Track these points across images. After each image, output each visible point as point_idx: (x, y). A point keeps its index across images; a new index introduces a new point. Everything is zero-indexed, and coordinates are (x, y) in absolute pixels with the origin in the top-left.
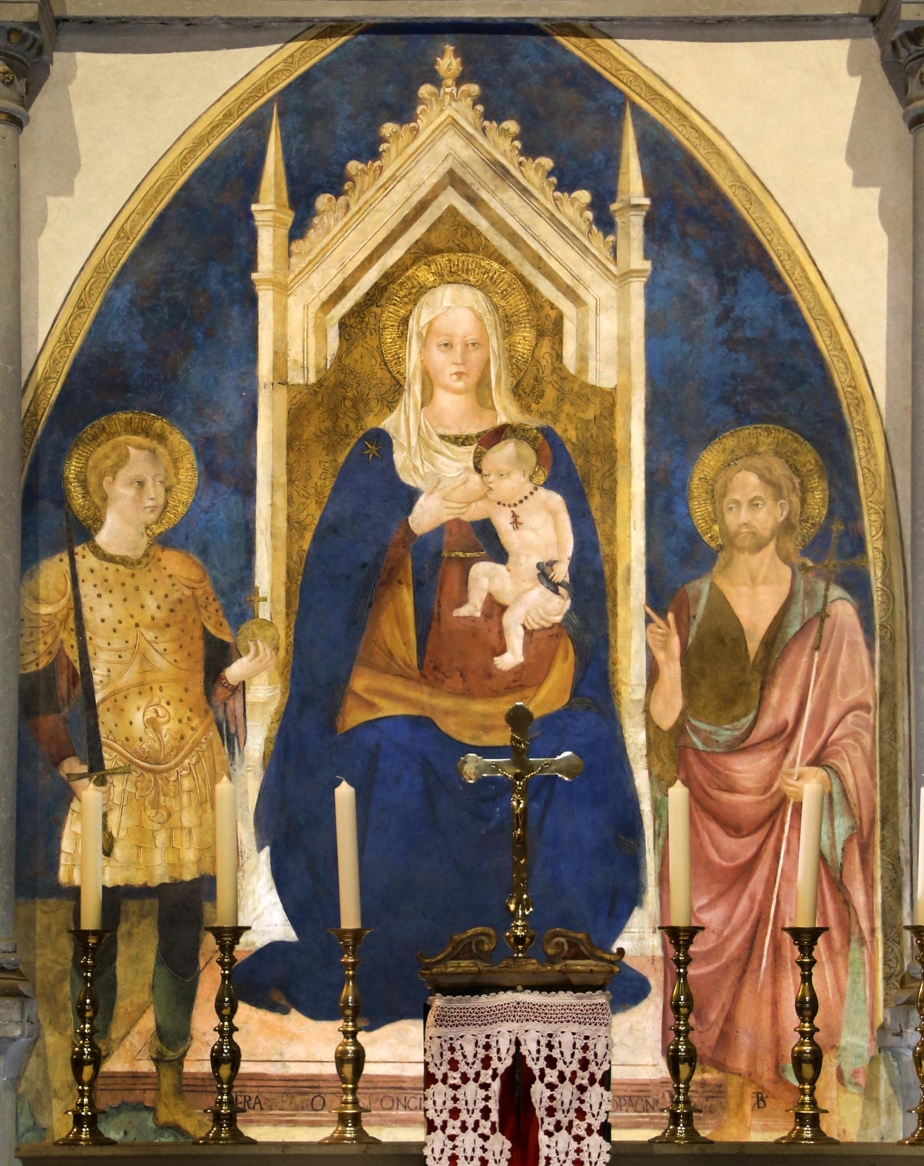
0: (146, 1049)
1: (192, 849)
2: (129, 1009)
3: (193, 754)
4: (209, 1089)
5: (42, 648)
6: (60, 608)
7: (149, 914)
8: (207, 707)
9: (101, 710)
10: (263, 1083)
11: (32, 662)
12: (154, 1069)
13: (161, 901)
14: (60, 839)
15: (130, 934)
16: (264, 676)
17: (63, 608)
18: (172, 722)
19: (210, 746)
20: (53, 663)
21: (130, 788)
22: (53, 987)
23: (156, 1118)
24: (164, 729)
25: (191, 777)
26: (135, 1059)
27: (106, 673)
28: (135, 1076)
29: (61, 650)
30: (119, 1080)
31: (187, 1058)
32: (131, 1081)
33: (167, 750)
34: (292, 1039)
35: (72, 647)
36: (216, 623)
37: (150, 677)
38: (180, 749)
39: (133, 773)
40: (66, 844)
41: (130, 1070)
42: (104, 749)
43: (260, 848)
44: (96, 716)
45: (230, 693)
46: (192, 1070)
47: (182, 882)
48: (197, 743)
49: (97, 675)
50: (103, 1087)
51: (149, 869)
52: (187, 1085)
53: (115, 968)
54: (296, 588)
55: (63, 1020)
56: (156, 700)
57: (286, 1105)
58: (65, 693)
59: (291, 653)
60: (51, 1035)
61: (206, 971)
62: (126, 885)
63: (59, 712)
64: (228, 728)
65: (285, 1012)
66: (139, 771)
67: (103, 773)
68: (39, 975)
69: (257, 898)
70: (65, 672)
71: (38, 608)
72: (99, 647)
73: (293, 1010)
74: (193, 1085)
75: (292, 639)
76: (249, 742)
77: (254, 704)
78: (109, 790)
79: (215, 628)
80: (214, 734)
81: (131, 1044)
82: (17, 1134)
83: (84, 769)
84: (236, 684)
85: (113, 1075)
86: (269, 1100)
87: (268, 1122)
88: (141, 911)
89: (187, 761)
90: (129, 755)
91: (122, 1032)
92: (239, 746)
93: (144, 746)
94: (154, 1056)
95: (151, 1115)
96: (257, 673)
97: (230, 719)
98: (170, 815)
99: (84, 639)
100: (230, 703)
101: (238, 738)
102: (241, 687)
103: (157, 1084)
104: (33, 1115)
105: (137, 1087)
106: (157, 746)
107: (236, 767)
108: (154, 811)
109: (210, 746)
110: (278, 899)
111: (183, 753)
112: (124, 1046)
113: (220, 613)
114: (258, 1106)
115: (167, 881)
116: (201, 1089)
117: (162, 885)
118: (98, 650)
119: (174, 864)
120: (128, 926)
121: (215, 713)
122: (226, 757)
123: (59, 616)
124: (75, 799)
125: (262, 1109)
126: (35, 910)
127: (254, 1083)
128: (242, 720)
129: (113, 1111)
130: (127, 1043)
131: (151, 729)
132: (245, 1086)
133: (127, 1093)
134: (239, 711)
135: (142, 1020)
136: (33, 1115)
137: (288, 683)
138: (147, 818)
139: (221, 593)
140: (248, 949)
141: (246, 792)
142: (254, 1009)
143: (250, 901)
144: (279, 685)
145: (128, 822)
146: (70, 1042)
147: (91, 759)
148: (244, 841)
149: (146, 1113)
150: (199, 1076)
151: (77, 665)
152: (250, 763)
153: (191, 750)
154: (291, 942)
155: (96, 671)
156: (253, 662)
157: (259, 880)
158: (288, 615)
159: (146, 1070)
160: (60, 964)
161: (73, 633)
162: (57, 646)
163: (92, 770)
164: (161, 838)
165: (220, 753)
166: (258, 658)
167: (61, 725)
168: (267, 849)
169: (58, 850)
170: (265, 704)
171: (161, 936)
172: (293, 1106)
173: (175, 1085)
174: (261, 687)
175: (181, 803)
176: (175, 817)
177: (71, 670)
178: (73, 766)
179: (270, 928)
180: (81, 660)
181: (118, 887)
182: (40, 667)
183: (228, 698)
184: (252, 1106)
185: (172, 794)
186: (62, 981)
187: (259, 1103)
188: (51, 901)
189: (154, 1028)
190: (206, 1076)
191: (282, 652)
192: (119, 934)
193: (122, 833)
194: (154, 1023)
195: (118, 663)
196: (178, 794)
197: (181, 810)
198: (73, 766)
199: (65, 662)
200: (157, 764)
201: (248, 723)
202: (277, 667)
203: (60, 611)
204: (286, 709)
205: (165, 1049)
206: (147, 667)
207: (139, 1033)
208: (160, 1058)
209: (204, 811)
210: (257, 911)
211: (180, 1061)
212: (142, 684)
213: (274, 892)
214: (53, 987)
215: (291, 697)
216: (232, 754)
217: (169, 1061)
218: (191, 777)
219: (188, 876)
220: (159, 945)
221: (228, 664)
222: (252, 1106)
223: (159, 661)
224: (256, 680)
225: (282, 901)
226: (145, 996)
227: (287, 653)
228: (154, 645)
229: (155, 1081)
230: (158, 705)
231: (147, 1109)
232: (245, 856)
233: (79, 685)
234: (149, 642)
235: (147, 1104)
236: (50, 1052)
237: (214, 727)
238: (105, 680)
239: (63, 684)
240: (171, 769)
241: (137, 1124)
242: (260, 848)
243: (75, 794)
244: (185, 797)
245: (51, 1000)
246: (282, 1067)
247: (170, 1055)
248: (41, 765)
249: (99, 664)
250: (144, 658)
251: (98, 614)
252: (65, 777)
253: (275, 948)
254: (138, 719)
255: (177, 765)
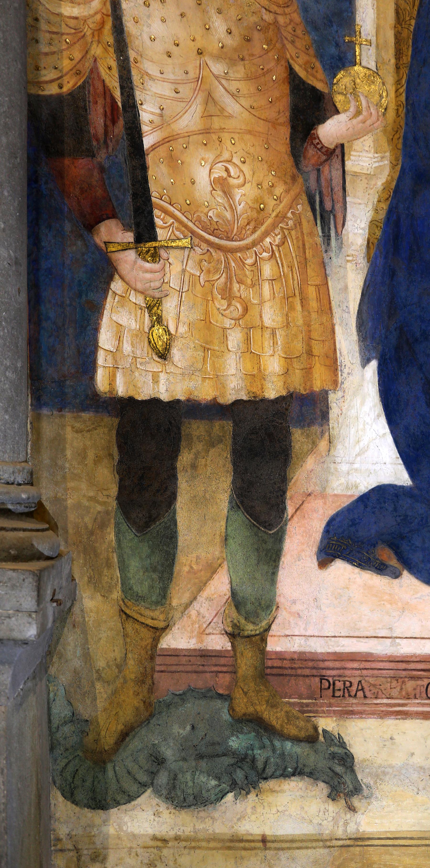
0: (218, 620)
1: (276, 357)
2: (195, 567)
3: (277, 231)
4: (299, 672)
5: (66, 64)
6: (92, 12)
7: (220, 441)
8: (295, 171)
9: (150, 160)
10: (368, 665)
11: (52, 81)
12: (228, 646)
13: (236, 424)
14: (96, 330)
15: (194, 466)
16: (367, 142)
17: (96, 13)
18: (247, 185)
19: (298, 223)
20: (82, 87)
21: (192, 269)
22: (92, 533)
23: (231, 709)
24: (238, 194)
25: (273, 261)
26: (202, 633)
27: (158, 111)
28: (204, 654)
29: (94, 70)
30: (184, 660)
31: (271, 633)
32: (200, 661)
33: (242, 222)
34: (403, 609)
35: (110, 68)
36: (306, 63)
37: (217, 123)
38: (259, 223)
39: (197, 248)
40: (105, 339)
41: (198, 646)
42: (156, 212)
43: (365, 362)
44: (144, 168)
45: (324, 157)
46: (278, 649)
47: (264, 400)
48: (282, 217)
49: (145, 111)
50: (162, 668)
51: (219, 379)
52: (272, 667)
53: (175, 513)
54: (407, 34)
55: (106, 579)
56: (226, 155)
57: (395, 693)
58: (101, 131)
59: (403, 115)
60: (92, 598)
61: (295, 518)
62: (188, 400)
63: (93, 156)
64: (321, 202)
65: (396, 575)
66: (204, 246)
67: (154, 244)
68: (72, 517)
69: (361, 426)
70: (101, 101)
71: (60, 6)
72: (148, 74)
73: (405, 574)
74: (280, 668)
75: (403, 98)
76: (349, 223)
77: (356, 175)
78: (163, 268)
79: (306, 70)
80: (302, 207)
81: (199, 613)
82: (50, 728)
83: (129, 237)
84: (332, 147)
85: (176, 653)
86: (374, 685)
87: (373, 714)
88: (209, 435)
89: (268, 240)
90: (190, 224)
91: (186, 598)
92: (336, 227)
93: (210, 214)
94: (229, 629)
95: (227, 703)
96: (357, 136)
97: (325, 191)
98: (246, 310)
99: (127, 59)
100: (326, 170)
101: (335, 217)
102: (338, 151)
103: (233, 665)
104: (70, 703)
105: (206, 668)
106: (228, 215)
107: (333, 255)
108: (225, 303)
109: (298, 223)
110: (387, 430)
111: (263, 228)
112: (189, 617)
113: (312, 52)
114: (360, 694)
115: (245, 398)
116: (289, 672)
117: (237, 403)
118: (146, 78)
119: (254, 375)
120: (192, 456)
121: (306, 181)
122: (319, 240)
123: (90, 22)
124: (117, 276)
125: (365, 697)
126: (63, 427)
127: (355, 665)
128: (341, 194)
129: (177, 699)
130: (193, 611)
131: (220, 193)
132: (345, 668)
133: (194, 676)
134: (337, 181)
135: (211, 582)
136: (70, 703)
137: (399, 153)
138: (215, 311)
139: (312, 24)
140: (349, 493)
141: (346, 288)
142: (357, 570)
143: (353, 431)
144: (388, 154)
145: (190, 315)
146: (117, 608)
147: (137, 225)
148: (345, 352)
149: (219, 702)
150: (288, 657)
151: (117, 94)
152: (350, 252)
153: (274, 226)
154: (402, 487)
155: (144, 107)
156: (355, 121)
157: (363, 403)
158: (397, 68)
159: (218, 648)
160: (98, 502)
161: (111, 50)
162: (88, 64)
163: (139, 240)
164: (235, 338)
165: (311, 234)
166: (361, 117)
167: (96, 173)
168: (374, 364)
169: (95, 346)
170: (369, 177)
171: (235, 471)
172: (404, 693)
173: (256, 668)
174: (364, 154)
175: (261, 295)
176: (254, 312)
177: (108, 100)
178: (113, 233)
179: (377, 467)
180: (122, 88)
181: (178, 401)
182: (65, 89)
183: (322, 164)
184: (353, 693)
185: (249, 282)
186: (103, 526)
187: (363, 689)
188: (85, 415)
189: (229, 594)
190: (296, 656)
191: (391, 114)
192: (179, 465)
193: (182, 329)
194: (228, 587)
195: (173, 99)
196: (256, 284)
197: (262, 303)
198: (113, 233)
199: (101, 88)
200: (228, 239)
201: (348, 199)
202: (385, 131)
203: (92, 16)
204: (397, 186)
205: (243, 621)
206: (212, 109)
207: (209, 599)
208: (236, 632)
209: (292, 308)
210: (361, 444)
211: (262, 637)
212: (207, 131)
213: (383, 421)
214: (92, 533)
215: (403, 171)
216: (327, 237)
217: (248, 637)
218: (273, 261)
219: (272, 393)
220: (233, 482)
221: (322, 120)
222: (353, 693)
223: (232, 106)
224: (357, 145)
225: (392, 432)
226: (216, 551)
227: (398, 115)
228: (224, 82)
229: (230, 661)
230: (229, 161)
231: (220, 696)
232: (346, 371)
233: (121, 122)
234: (217, 77)
235: (221, 691)
236: (91, 619)
237: (304, 197)
238: (157, 120)
239: (97, 119)
240: (248, 248)
241: (207, 716)
242: (365, 362)
243: (116, 270)
244: (266, 288)
245: (90, 551)
246: (392, 645)
247: (250, 628)
248: (68, 227)
249: (148, 98)
250: (210, 98)
251: (145, 28)
252: (103, 245)
253: (382, 495)
254: (202, 176)
255: (254, 244)
